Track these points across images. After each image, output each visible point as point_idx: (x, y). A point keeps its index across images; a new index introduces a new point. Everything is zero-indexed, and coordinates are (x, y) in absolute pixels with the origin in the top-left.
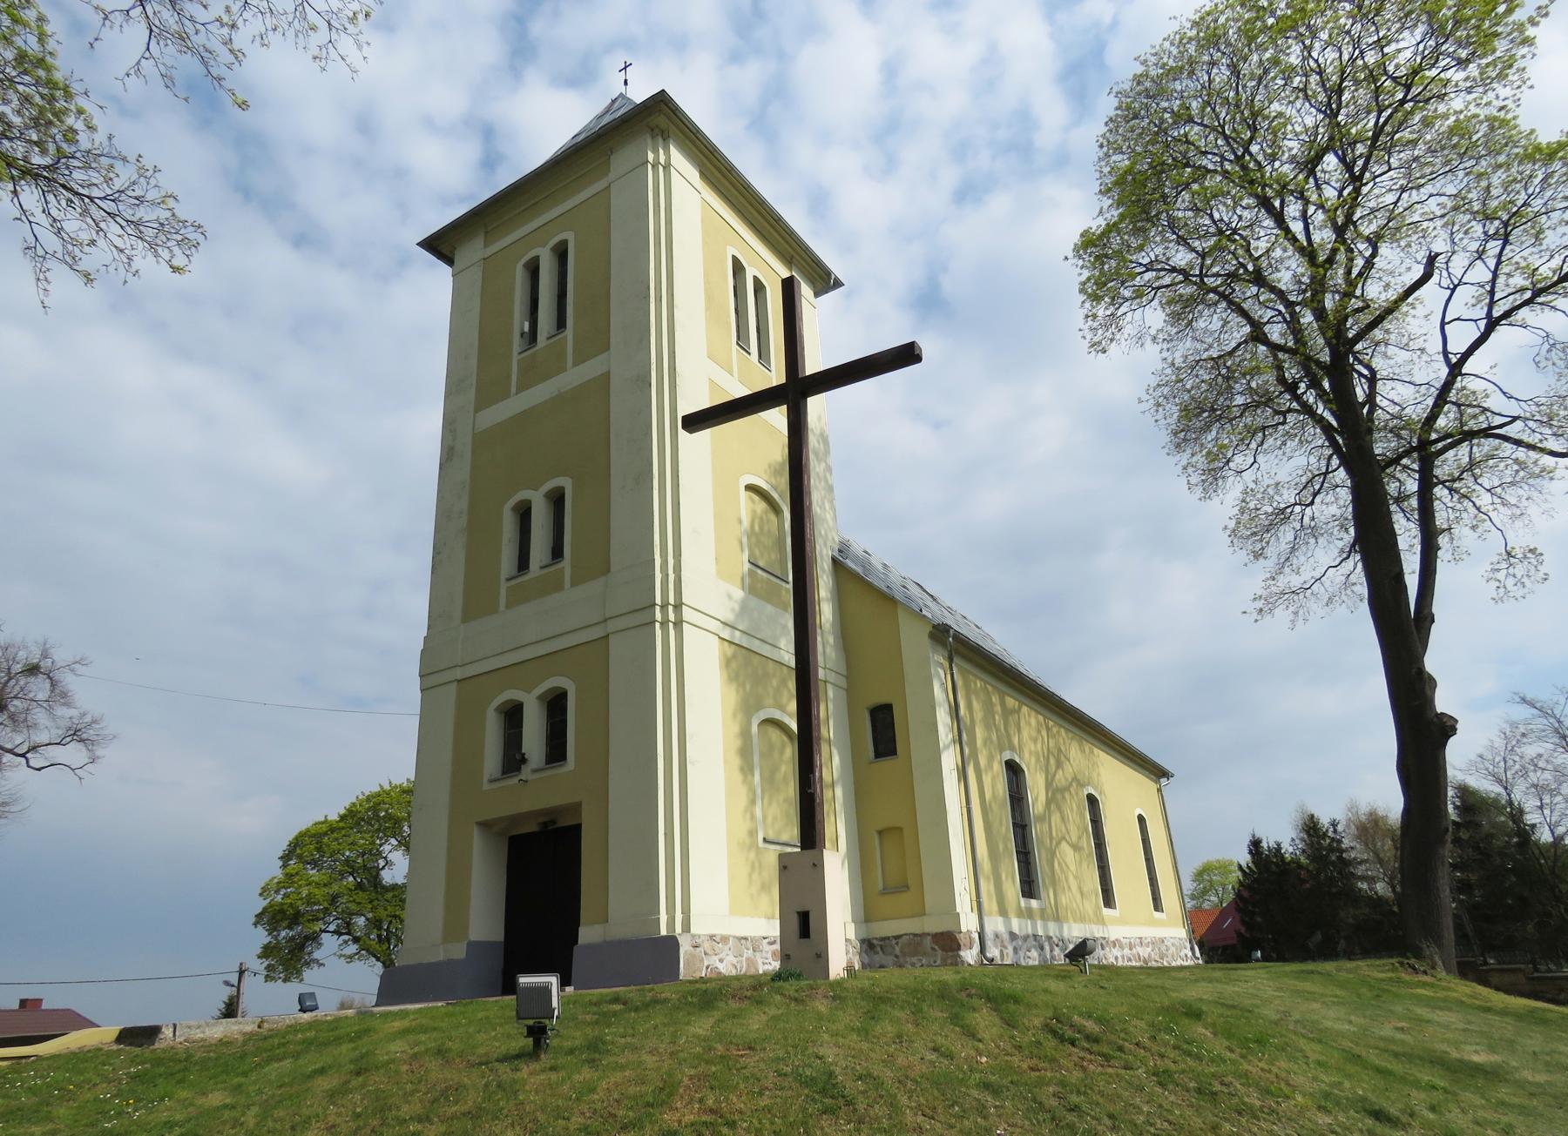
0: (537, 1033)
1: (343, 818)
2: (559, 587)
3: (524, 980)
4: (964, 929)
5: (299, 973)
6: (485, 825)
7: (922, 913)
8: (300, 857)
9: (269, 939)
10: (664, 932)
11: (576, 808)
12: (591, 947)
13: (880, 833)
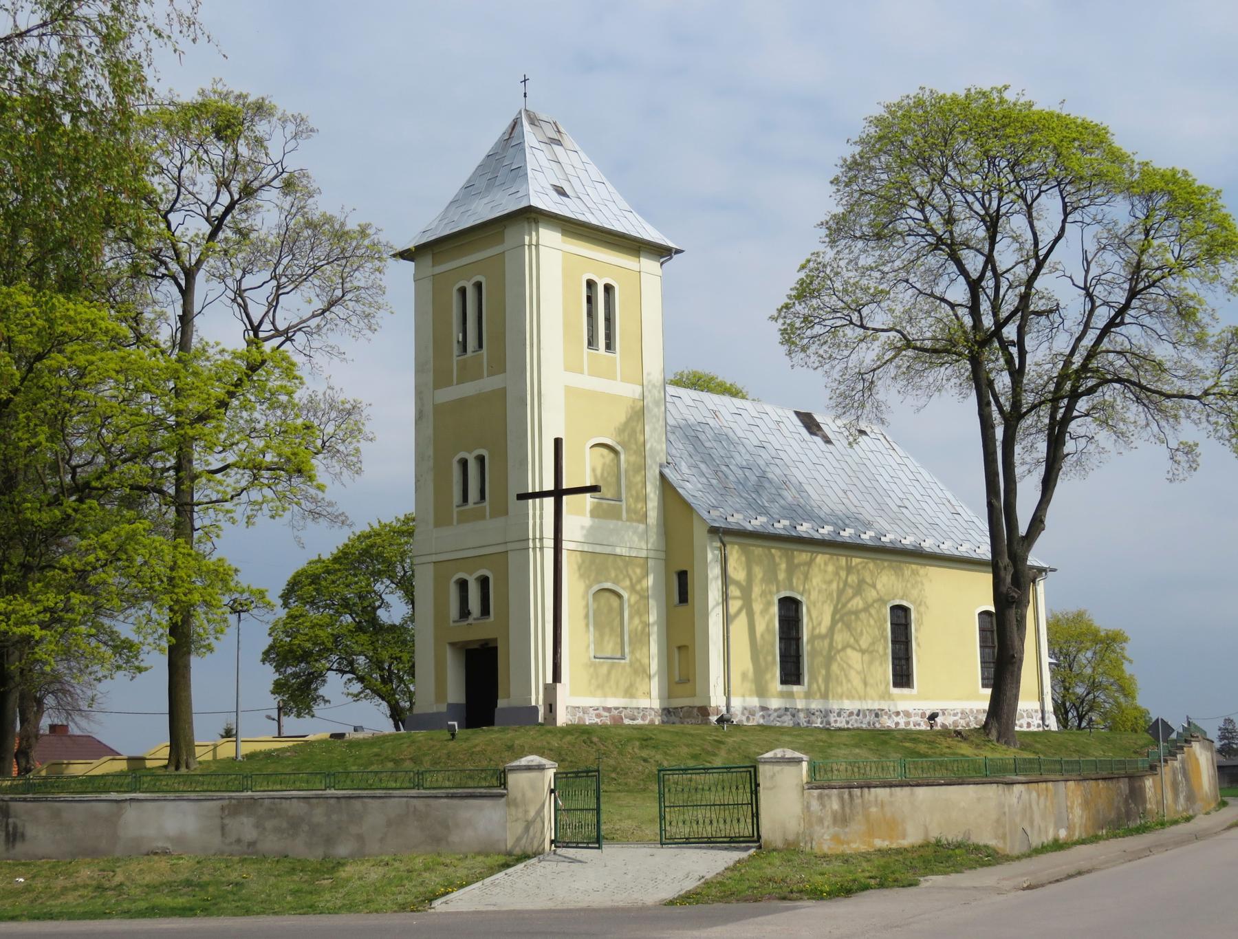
0: (453, 735)
1: (336, 560)
2: (483, 517)
3: (540, 720)
4: (713, 704)
5: (309, 708)
6: (453, 644)
7: (694, 695)
8: (300, 598)
9: (277, 676)
10: (533, 704)
11: (495, 640)
12: (503, 709)
13: (679, 648)
